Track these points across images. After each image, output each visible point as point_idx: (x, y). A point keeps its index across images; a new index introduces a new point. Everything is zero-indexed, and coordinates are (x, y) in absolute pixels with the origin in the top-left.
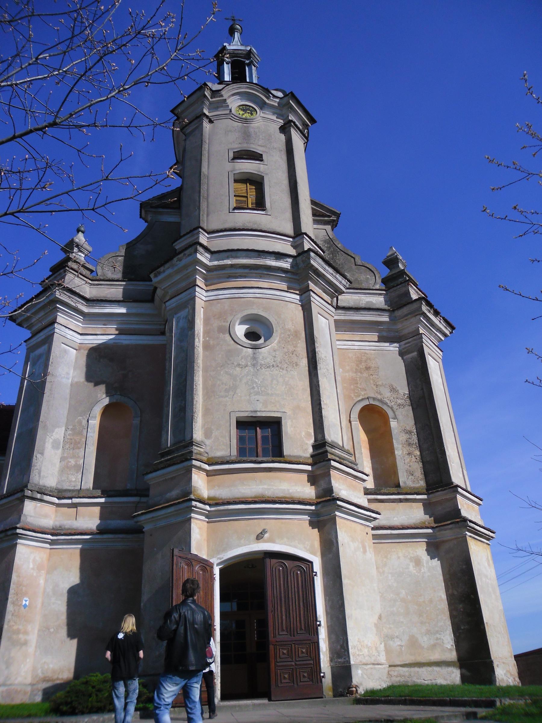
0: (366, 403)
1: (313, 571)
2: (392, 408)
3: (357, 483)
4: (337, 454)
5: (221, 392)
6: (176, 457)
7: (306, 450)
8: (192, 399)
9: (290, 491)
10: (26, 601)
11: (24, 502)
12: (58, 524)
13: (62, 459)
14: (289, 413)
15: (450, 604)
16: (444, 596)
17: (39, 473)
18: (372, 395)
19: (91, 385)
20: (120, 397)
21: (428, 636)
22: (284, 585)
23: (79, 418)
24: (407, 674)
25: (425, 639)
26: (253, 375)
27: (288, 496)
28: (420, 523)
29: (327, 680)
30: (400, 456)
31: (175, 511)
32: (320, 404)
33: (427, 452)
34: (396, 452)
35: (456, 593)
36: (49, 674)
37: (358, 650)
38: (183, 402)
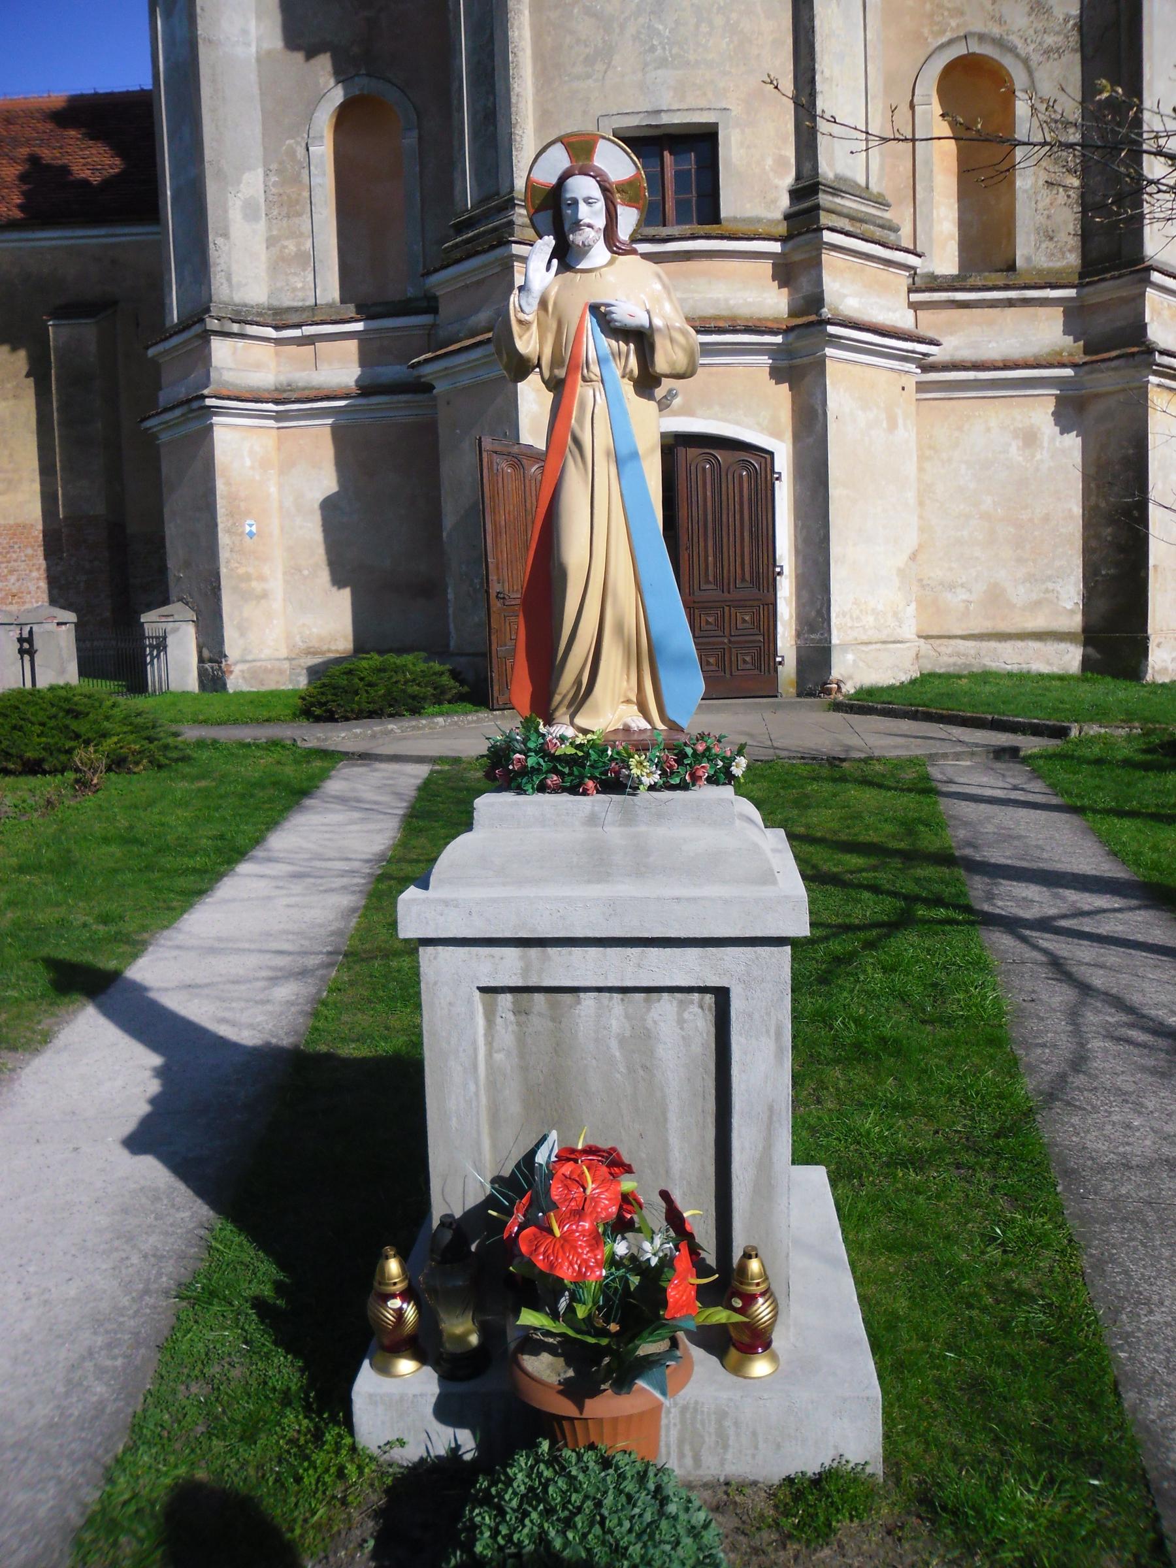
0: (959, 50)
1: (773, 471)
2: (1026, 62)
3: (892, 276)
4: (845, 211)
5: (574, 64)
6: (484, 232)
7: (774, 201)
8: (508, 90)
9: (732, 302)
10: (251, 526)
11: (209, 342)
12: (283, 379)
13: (271, 242)
14: (736, 110)
15: (1087, 525)
16: (1077, 510)
17: (229, 280)
18: (978, 27)
19: (299, 56)
20: (365, 81)
21: (1028, 585)
22: (713, 497)
23: (288, 142)
24: (972, 652)
25: (1021, 590)
26: (652, 12)
27: (725, 313)
28: (1048, 354)
29: (788, 669)
30: (1026, 191)
31: (485, 356)
32: (813, 81)
33: (1099, 178)
34: (1018, 183)
35: (1103, 505)
36: (314, 643)
37: (851, 617)
38: (491, 99)
